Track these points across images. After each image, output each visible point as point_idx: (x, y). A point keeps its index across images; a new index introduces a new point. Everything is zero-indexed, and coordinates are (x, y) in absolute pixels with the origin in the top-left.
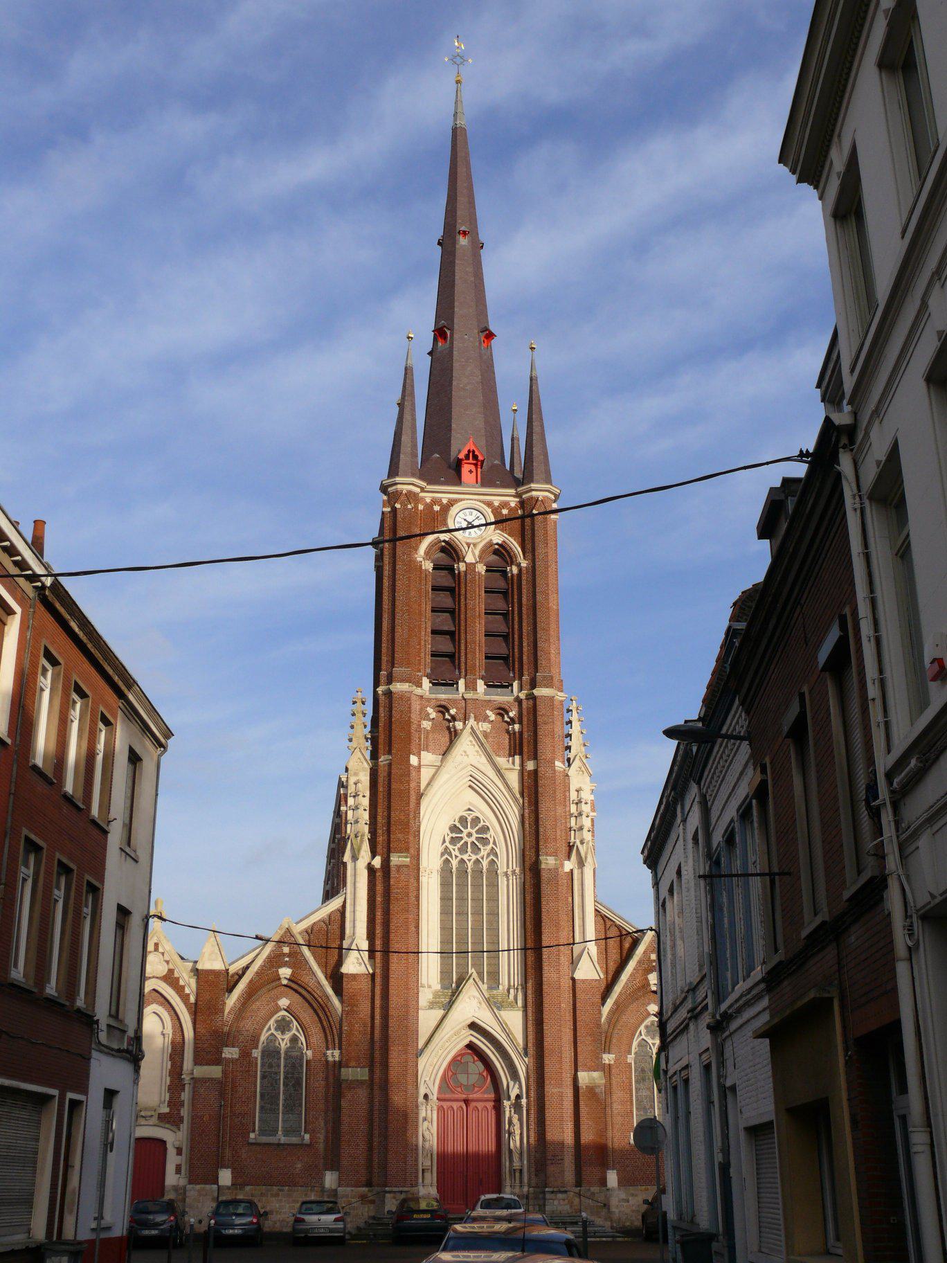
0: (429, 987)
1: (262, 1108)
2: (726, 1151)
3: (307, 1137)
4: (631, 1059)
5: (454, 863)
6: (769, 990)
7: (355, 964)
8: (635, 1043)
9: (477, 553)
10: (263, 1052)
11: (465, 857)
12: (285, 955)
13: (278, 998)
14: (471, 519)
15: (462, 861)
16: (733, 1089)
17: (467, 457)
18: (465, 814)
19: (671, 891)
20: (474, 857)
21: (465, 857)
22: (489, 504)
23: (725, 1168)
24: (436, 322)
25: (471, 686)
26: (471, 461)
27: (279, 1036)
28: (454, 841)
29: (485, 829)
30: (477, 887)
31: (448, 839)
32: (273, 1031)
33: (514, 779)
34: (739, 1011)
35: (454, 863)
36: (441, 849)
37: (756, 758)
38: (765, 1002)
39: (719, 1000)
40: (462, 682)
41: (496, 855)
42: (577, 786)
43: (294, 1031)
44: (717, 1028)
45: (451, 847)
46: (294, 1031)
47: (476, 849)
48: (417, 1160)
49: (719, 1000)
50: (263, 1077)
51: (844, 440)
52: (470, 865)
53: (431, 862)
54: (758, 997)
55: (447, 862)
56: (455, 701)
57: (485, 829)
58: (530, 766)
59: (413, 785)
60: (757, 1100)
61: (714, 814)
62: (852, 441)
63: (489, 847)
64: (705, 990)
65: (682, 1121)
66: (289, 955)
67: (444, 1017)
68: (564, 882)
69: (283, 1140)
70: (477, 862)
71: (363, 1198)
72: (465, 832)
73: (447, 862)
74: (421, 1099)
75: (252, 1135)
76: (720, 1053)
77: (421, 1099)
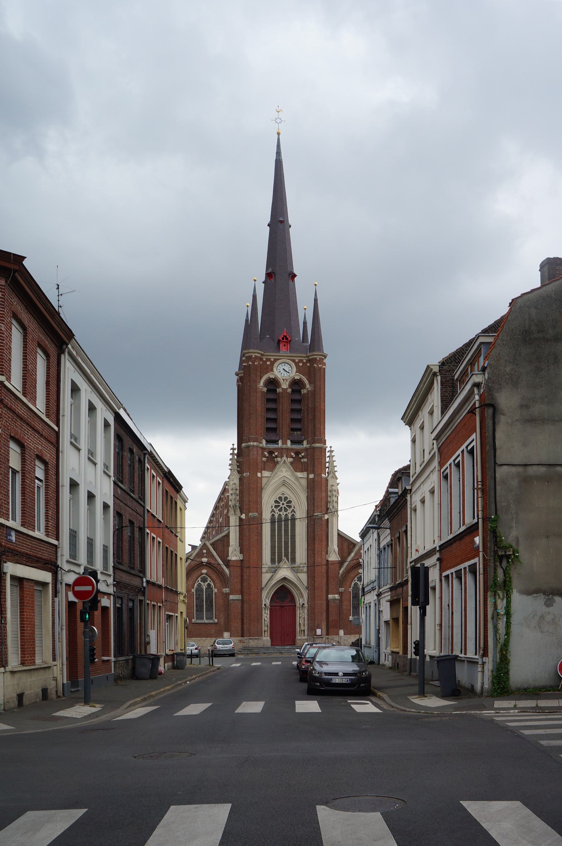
0: (266, 564)
1: (197, 610)
2: (379, 626)
3: (216, 620)
4: (351, 590)
5: (276, 515)
6: (391, 591)
7: (234, 555)
8: (353, 584)
9: (287, 383)
10: (196, 590)
11: (281, 513)
12: (204, 553)
13: (202, 570)
14: (284, 371)
15: (280, 514)
16: (382, 611)
17: (283, 339)
18: (281, 496)
19: (368, 549)
20: (285, 513)
21: (281, 513)
22: (293, 361)
23: (379, 630)
24: (266, 271)
25: (284, 443)
26: (285, 340)
27: (202, 584)
28: (276, 507)
29: (290, 502)
30: (286, 526)
31: (273, 506)
32: (200, 582)
33: (304, 482)
34: (384, 593)
35: (276, 515)
36: (271, 510)
37: (392, 534)
38: (389, 593)
39: (379, 588)
40: (280, 442)
41: (295, 512)
42: (332, 484)
43: (209, 582)
44: (379, 595)
45: (275, 509)
46: (209, 582)
47: (286, 510)
48: (262, 627)
49: (379, 588)
50: (196, 599)
51: (409, 492)
52: (283, 516)
53: (266, 516)
54: (388, 591)
55: (273, 515)
56: (277, 449)
57: (290, 502)
58: (311, 476)
59: (259, 485)
60: (386, 615)
61: (381, 539)
62: (411, 492)
63: (291, 509)
64: (376, 584)
65: (368, 617)
66: (206, 553)
67: (272, 576)
68: (324, 523)
69: (206, 621)
70: (286, 515)
71: (240, 641)
72: (281, 503)
73: (273, 515)
74: (263, 606)
75: (193, 620)
76: (379, 602)
77: (263, 606)
